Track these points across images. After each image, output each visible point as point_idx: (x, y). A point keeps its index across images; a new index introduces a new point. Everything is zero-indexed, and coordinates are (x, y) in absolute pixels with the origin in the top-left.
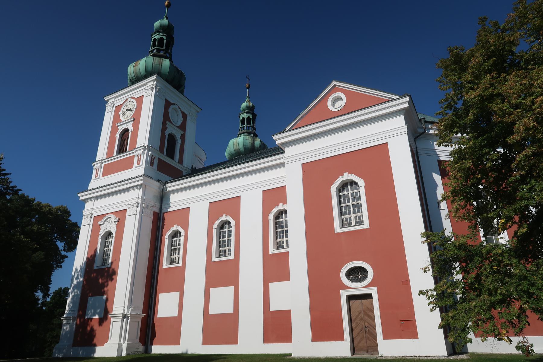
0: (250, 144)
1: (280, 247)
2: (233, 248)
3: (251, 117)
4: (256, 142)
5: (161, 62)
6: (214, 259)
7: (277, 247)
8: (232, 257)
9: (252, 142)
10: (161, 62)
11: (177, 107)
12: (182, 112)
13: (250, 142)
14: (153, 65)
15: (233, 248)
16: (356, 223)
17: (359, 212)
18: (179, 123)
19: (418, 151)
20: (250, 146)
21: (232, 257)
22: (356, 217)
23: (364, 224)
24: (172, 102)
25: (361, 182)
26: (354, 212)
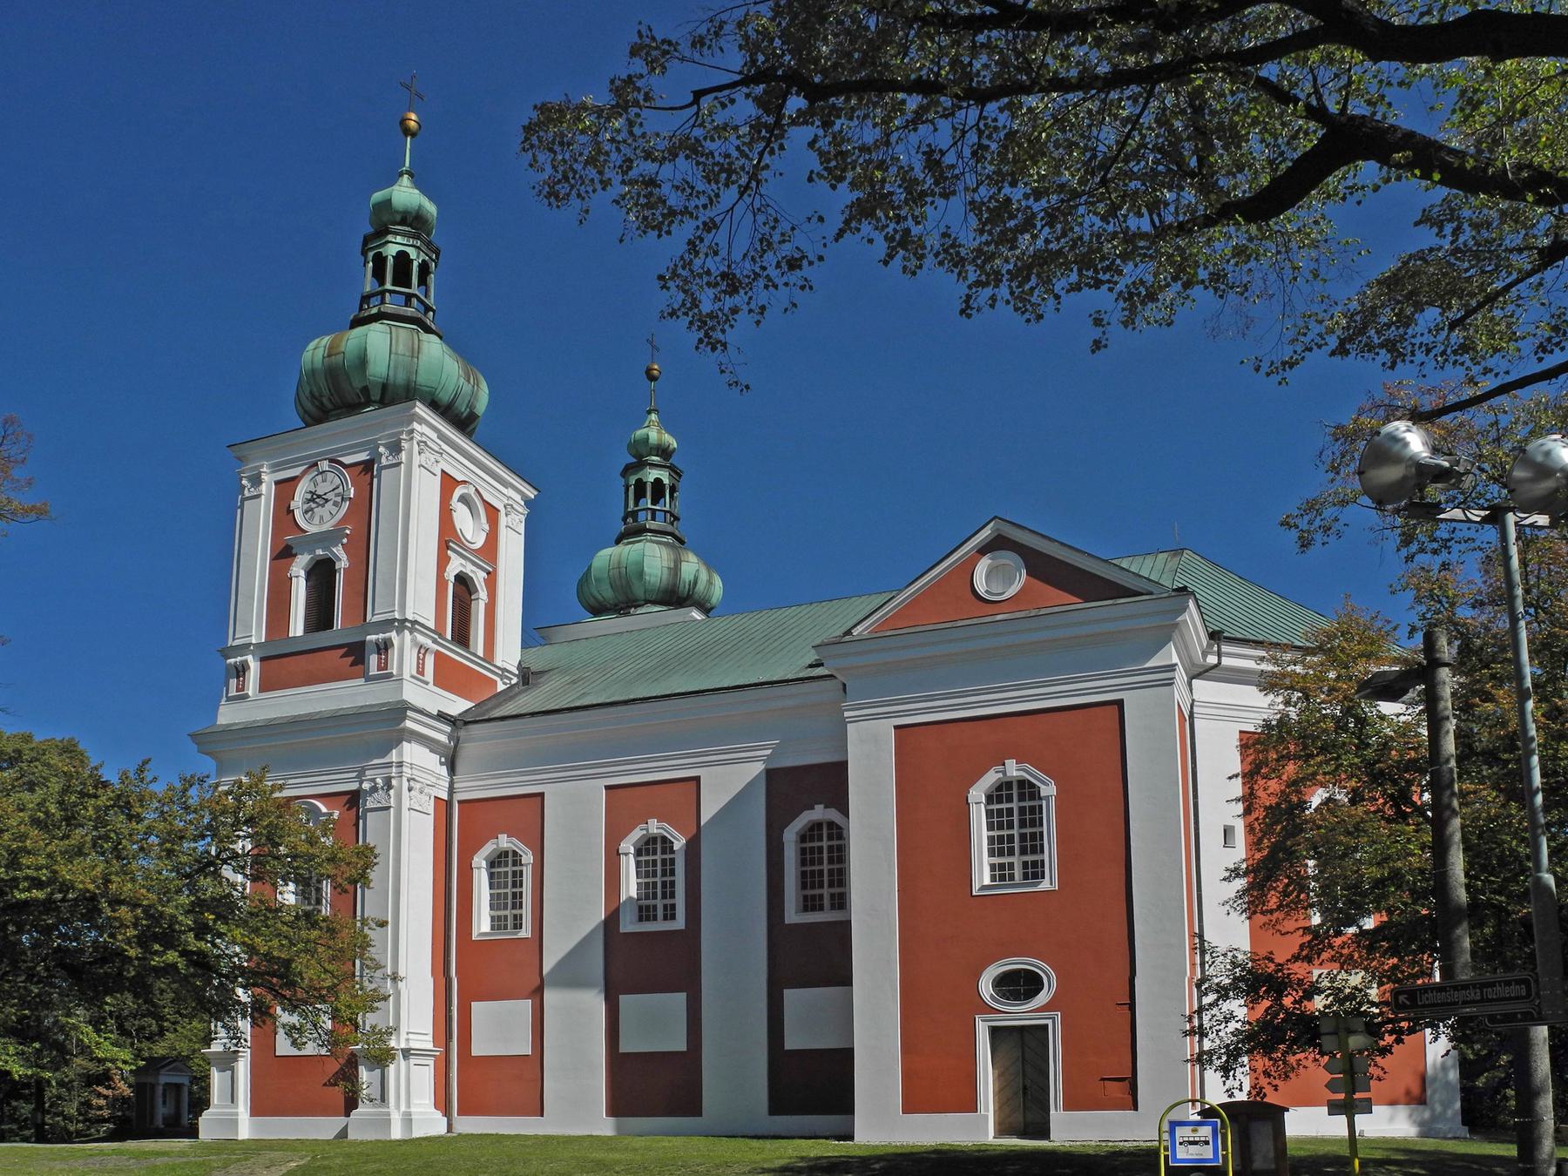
0: (666, 571)
1: (648, 919)
2: (527, 912)
3: (666, 481)
4: (684, 566)
5: (416, 346)
6: (792, 915)
7: (641, 919)
8: (679, 923)
9: (672, 565)
10: (416, 346)
11: (472, 491)
12: (487, 504)
13: (665, 564)
14: (392, 356)
15: (527, 912)
16: (1026, 876)
17: (1034, 851)
18: (479, 541)
19: (1196, 710)
20: (665, 576)
21: (679, 923)
22: (1025, 864)
23: (1241, 732)
24: (460, 478)
25: (1049, 790)
26: (1023, 852)
